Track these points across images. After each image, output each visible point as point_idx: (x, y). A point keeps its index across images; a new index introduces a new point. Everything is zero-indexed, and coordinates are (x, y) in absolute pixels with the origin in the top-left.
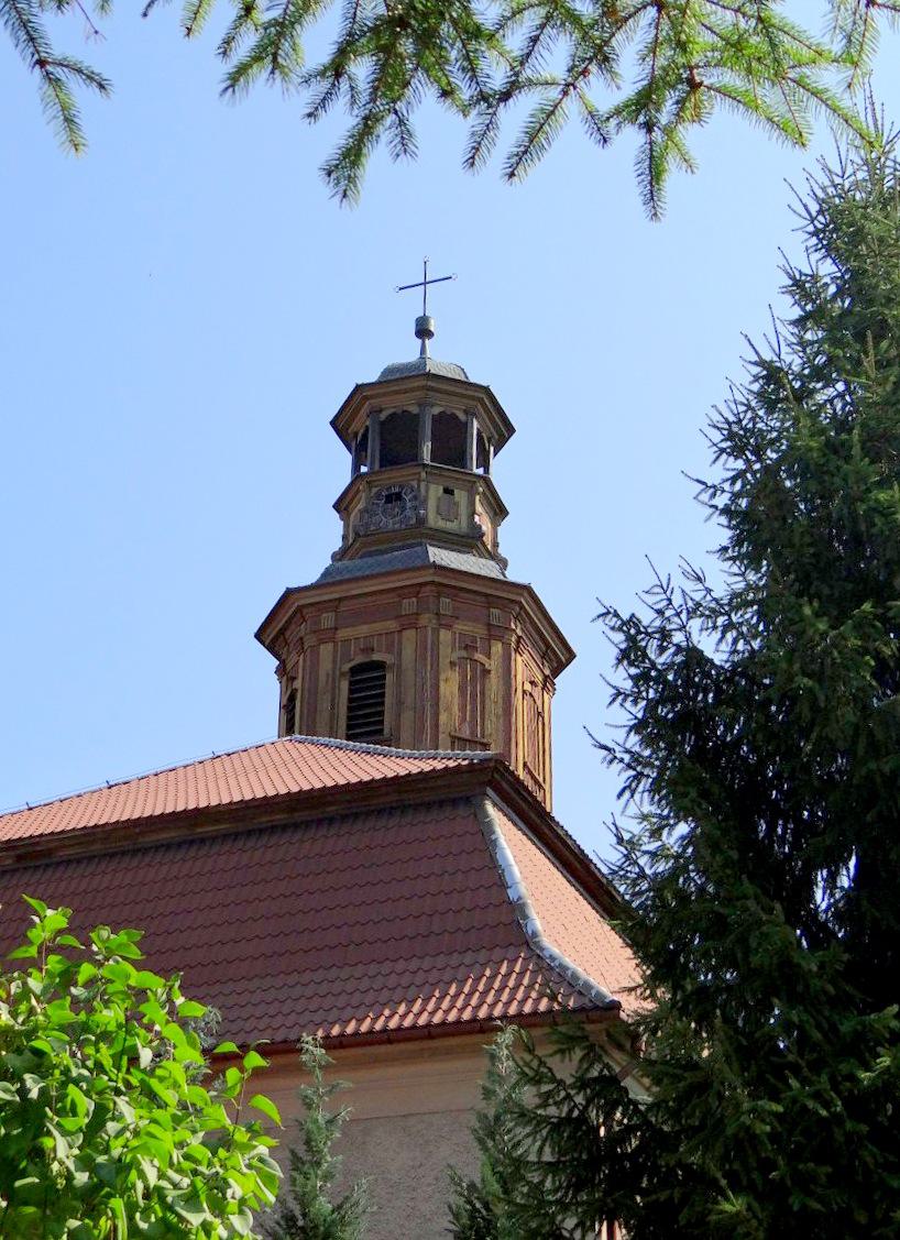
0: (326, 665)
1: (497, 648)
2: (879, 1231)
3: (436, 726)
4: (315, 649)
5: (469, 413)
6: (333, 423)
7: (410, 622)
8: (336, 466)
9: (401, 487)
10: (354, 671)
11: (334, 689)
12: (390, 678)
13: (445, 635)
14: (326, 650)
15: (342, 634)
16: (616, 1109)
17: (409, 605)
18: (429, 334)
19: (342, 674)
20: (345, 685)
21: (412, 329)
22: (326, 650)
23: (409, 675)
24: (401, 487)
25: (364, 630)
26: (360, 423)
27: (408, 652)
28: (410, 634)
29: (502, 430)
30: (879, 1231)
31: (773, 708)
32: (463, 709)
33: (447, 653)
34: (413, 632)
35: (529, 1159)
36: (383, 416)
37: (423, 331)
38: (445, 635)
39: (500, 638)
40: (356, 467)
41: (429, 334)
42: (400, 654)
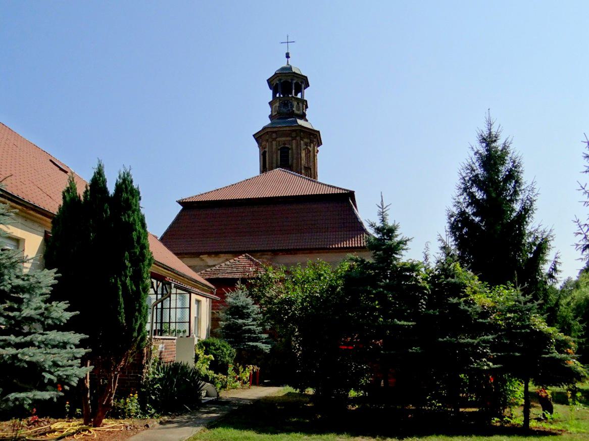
0: (274, 147)
1: (312, 145)
2: (496, 366)
3: (301, 164)
4: (272, 142)
5: (302, 82)
6: (267, 80)
7: (294, 138)
8: (269, 94)
9: (288, 101)
10: (281, 149)
11: (277, 153)
12: (290, 151)
13: (302, 142)
14: (274, 143)
15: (278, 139)
16: (504, 331)
17: (294, 134)
18: (289, 57)
19: (279, 150)
20: (279, 152)
21: (285, 56)
22: (274, 143)
23: (294, 151)
24: (288, 101)
25: (284, 139)
26: (276, 81)
27: (294, 146)
28: (294, 141)
29: (307, 85)
30: (496, 366)
31: (409, 311)
32: (306, 160)
33: (303, 147)
34: (275, 142)
35: (572, 333)
36: (282, 81)
37: (288, 56)
38: (302, 142)
39: (312, 143)
40: (274, 95)
41: (289, 57)
42: (292, 146)
